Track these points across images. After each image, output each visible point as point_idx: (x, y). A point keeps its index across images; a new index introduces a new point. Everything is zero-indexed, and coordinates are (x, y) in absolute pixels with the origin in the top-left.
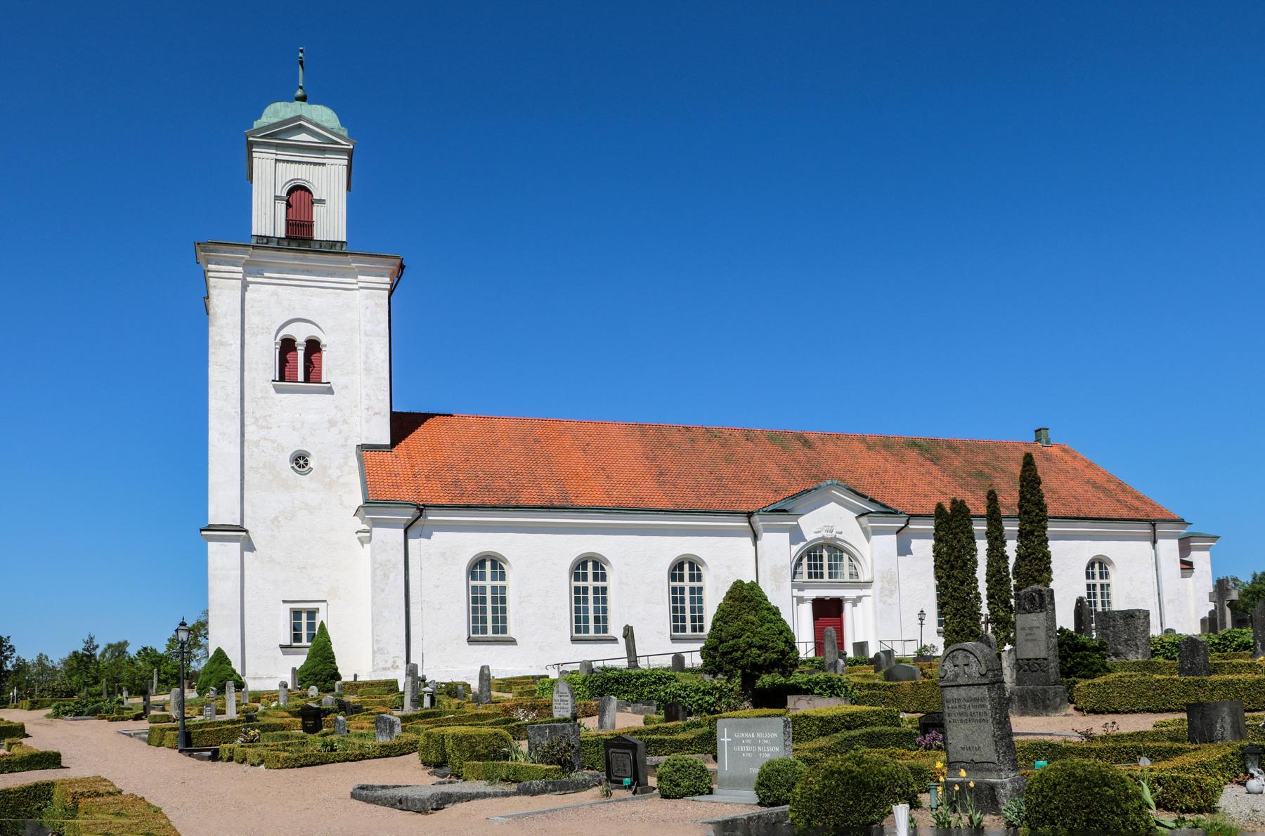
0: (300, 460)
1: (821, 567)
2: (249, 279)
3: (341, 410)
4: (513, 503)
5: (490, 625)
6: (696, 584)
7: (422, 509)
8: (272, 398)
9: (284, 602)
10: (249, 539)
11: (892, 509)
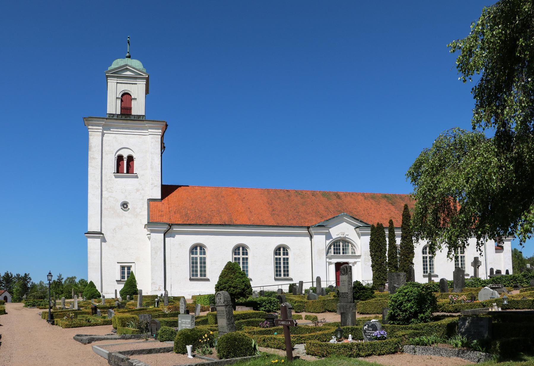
0: (125, 205)
1: (339, 250)
2: (105, 132)
4: (209, 223)
5: (199, 273)
6: (286, 257)
7: (171, 226)
8: (113, 180)
9: (118, 263)
10: (104, 237)
11: (369, 225)
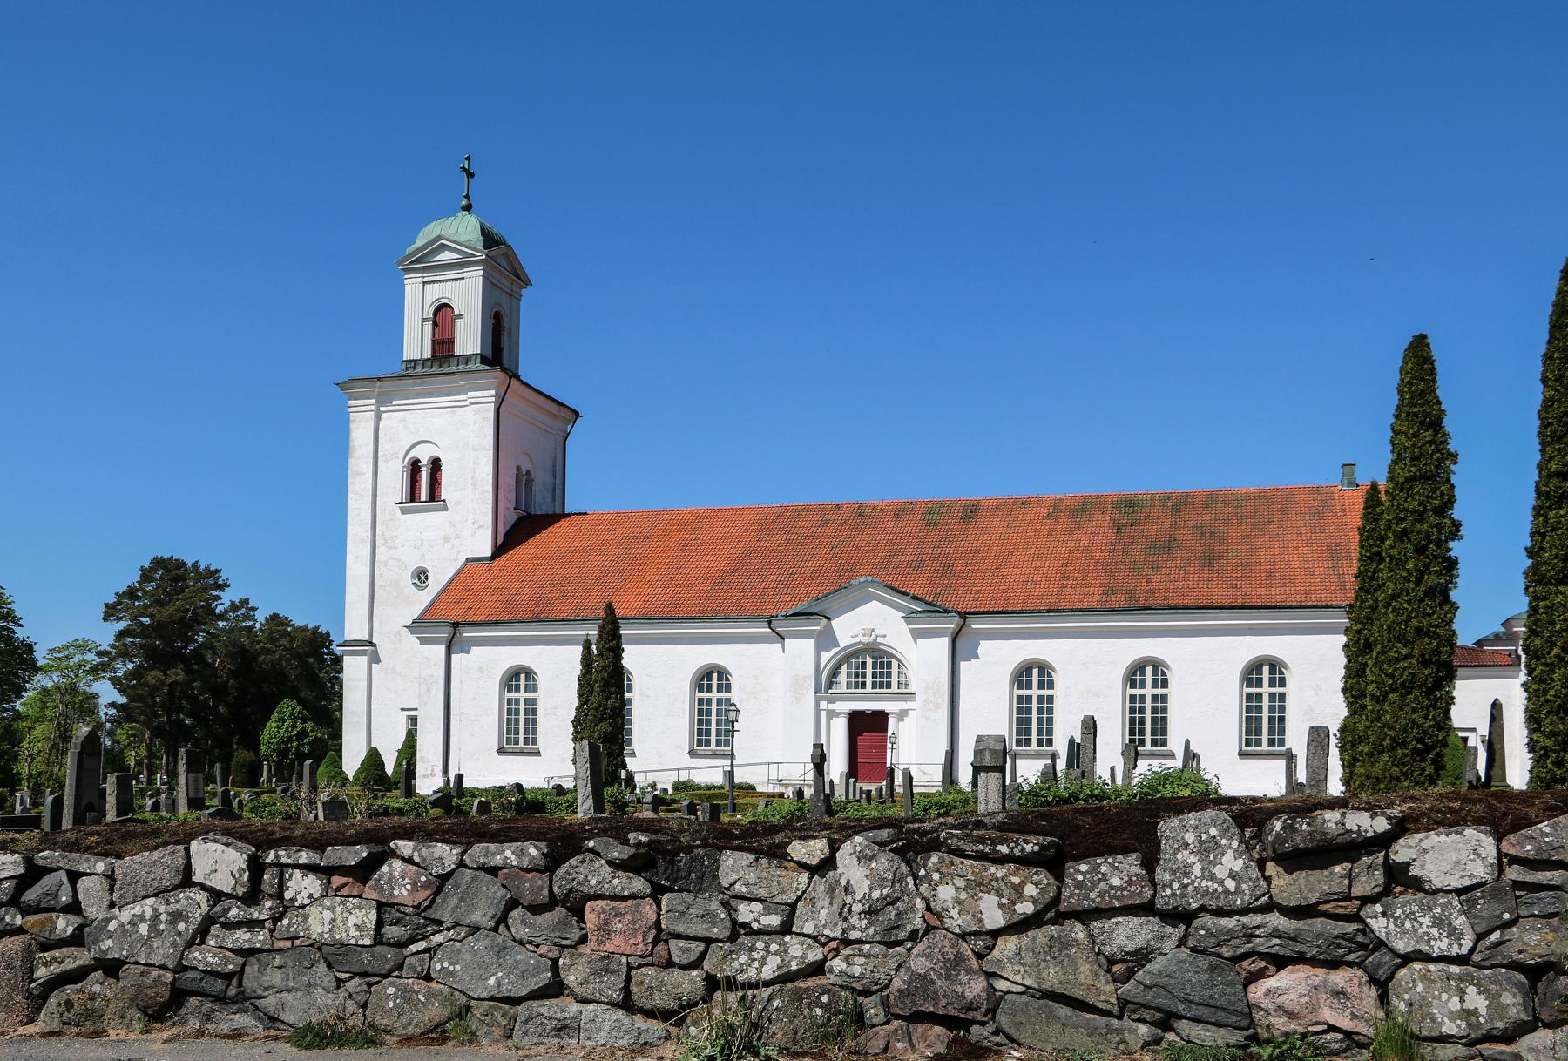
2: (382, 409)
3: (454, 526)
6: (1046, 692)
7: (456, 626)
9: (402, 709)
